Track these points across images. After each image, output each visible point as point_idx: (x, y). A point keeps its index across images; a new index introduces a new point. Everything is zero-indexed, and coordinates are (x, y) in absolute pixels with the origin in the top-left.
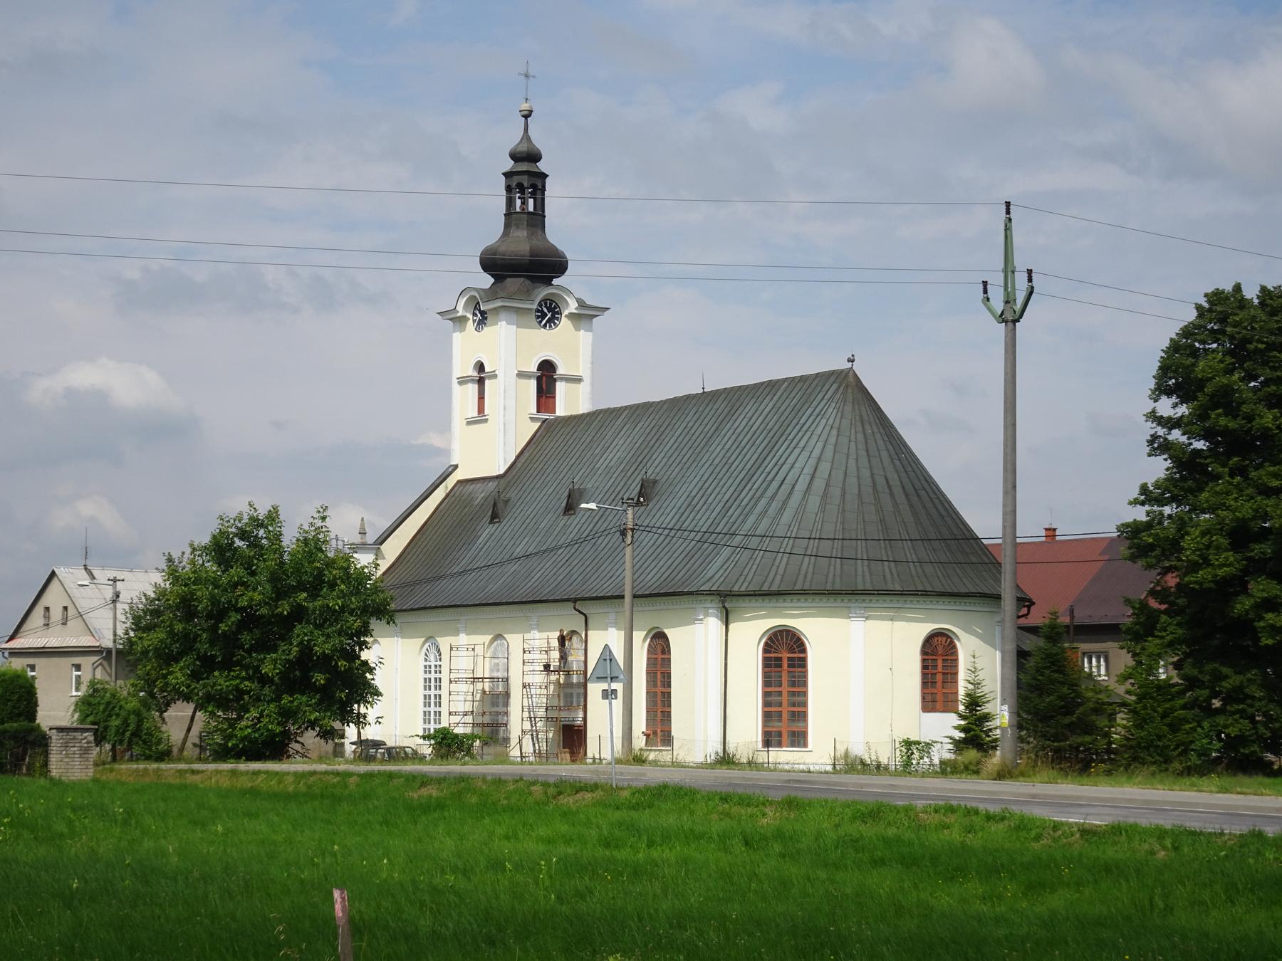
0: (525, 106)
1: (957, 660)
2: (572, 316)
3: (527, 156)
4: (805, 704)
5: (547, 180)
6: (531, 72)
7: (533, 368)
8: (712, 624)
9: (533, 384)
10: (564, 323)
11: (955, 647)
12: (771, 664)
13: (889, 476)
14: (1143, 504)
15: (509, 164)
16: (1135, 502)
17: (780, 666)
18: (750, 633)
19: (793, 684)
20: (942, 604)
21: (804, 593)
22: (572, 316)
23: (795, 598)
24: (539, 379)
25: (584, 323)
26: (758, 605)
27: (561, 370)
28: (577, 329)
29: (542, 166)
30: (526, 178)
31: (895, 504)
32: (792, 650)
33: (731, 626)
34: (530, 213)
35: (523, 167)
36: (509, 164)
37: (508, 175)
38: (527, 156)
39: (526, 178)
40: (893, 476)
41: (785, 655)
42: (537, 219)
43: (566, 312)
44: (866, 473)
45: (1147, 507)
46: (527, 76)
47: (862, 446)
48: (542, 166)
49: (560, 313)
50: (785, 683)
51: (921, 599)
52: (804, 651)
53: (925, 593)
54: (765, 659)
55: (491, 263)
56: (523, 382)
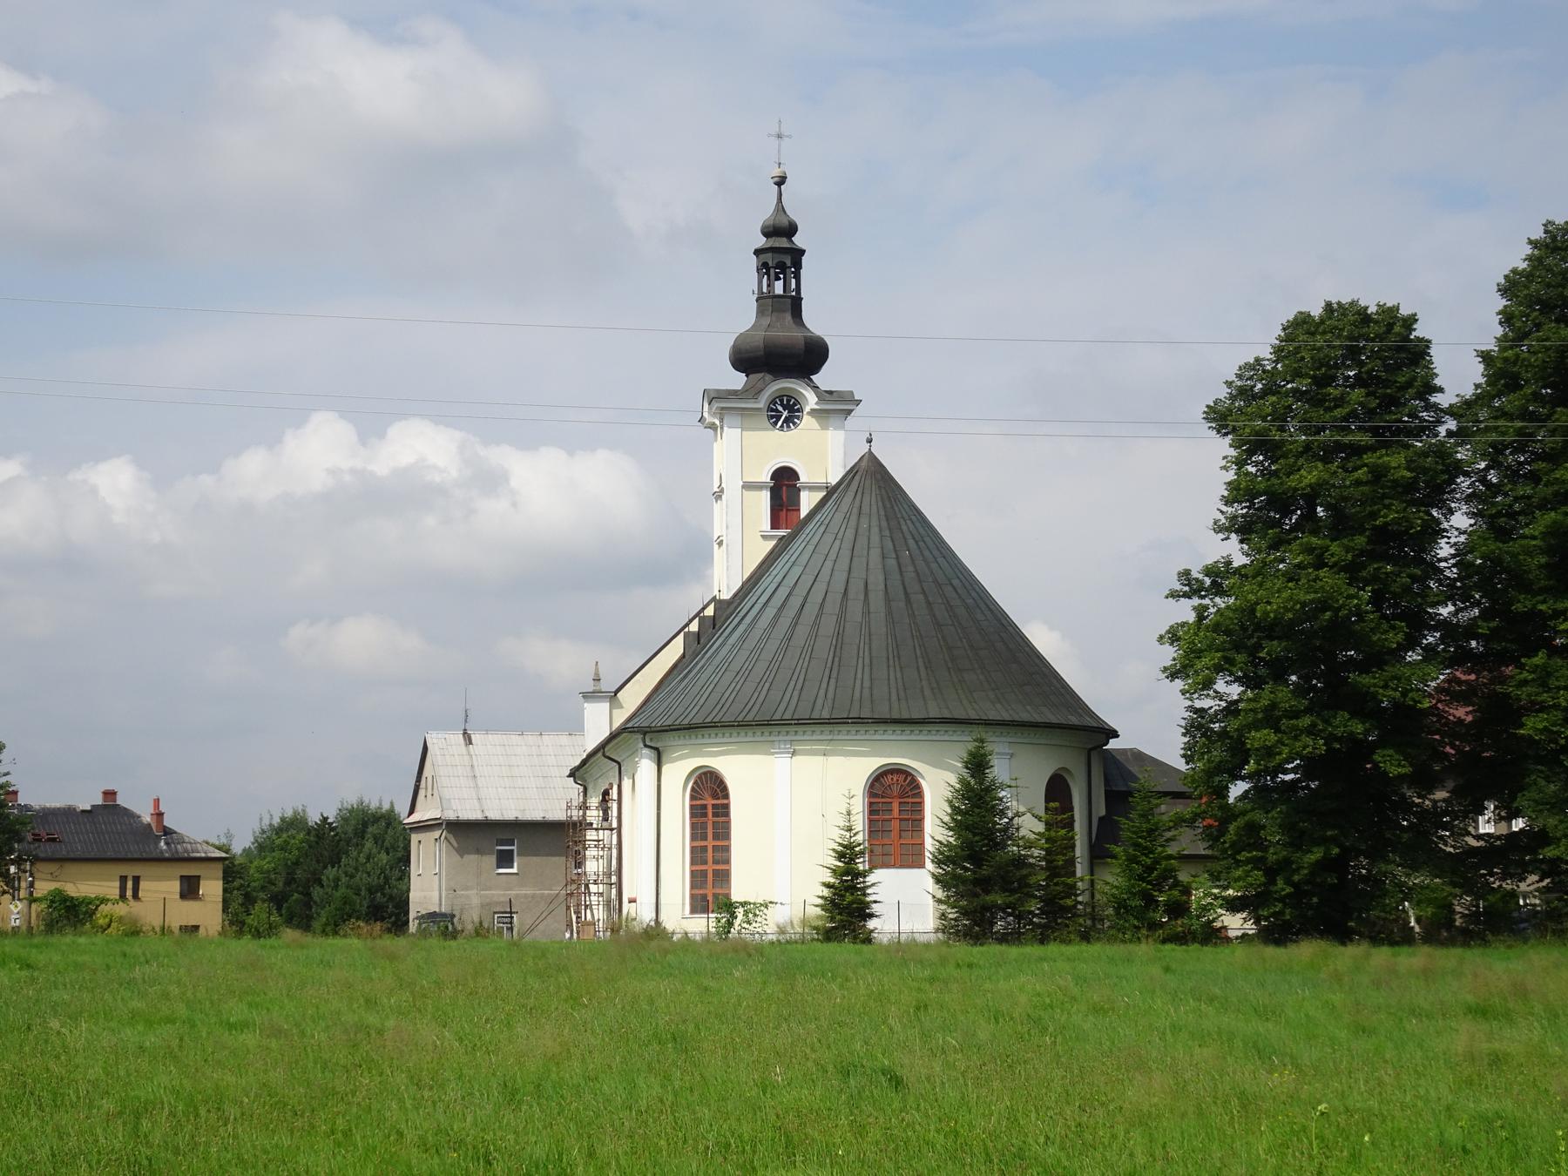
0: (777, 172)
1: (921, 803)
2: (813, 412)
3: (781, 230)
4: (728, 862)
5: (804, 259)
6: (785, 131)
7: (765, 477)
8: (645, 766)
9: (765, 497)
10: (807, 421)
11: (918, 787)
12: (697, 812)
13: (871, 579)
14: (1186, 595)
15: (761, 241)
16: (1174, 595)
17: (705, 815)
18: (679, 771)
19: (716, 837)
20: (891, 733)
21: (713, 725)
22: (813, 412)
23: (713, 731)
24: (772, 490)
25: (834, 420)
26: (700, 741)
27: (803, 478)
28: (824, 427)
29: (798, 240)
30: (781, 254)
31: (867, 612)
32: (715, 796)
33: (665, 768)
34: (779, 296)
35: (782, 243)
36: (761, 241)
37: (757, 252)
38: (781, 230)
39: (781, 254)
40: (877, 580)
41: (710, 802)
42: (795, 305)
43: (807, 409)
44: (840, 578)
45: (1196, 601)
46: (779, 136)
47: (847, 545)
48: (798, 240)
49: (801, 410)
50: (710, 836)
51: (853, 728)
52: (727, 796)
53: (859, 721)
54: (692, 807)
55: (744, 360)
56: (751, 495)
